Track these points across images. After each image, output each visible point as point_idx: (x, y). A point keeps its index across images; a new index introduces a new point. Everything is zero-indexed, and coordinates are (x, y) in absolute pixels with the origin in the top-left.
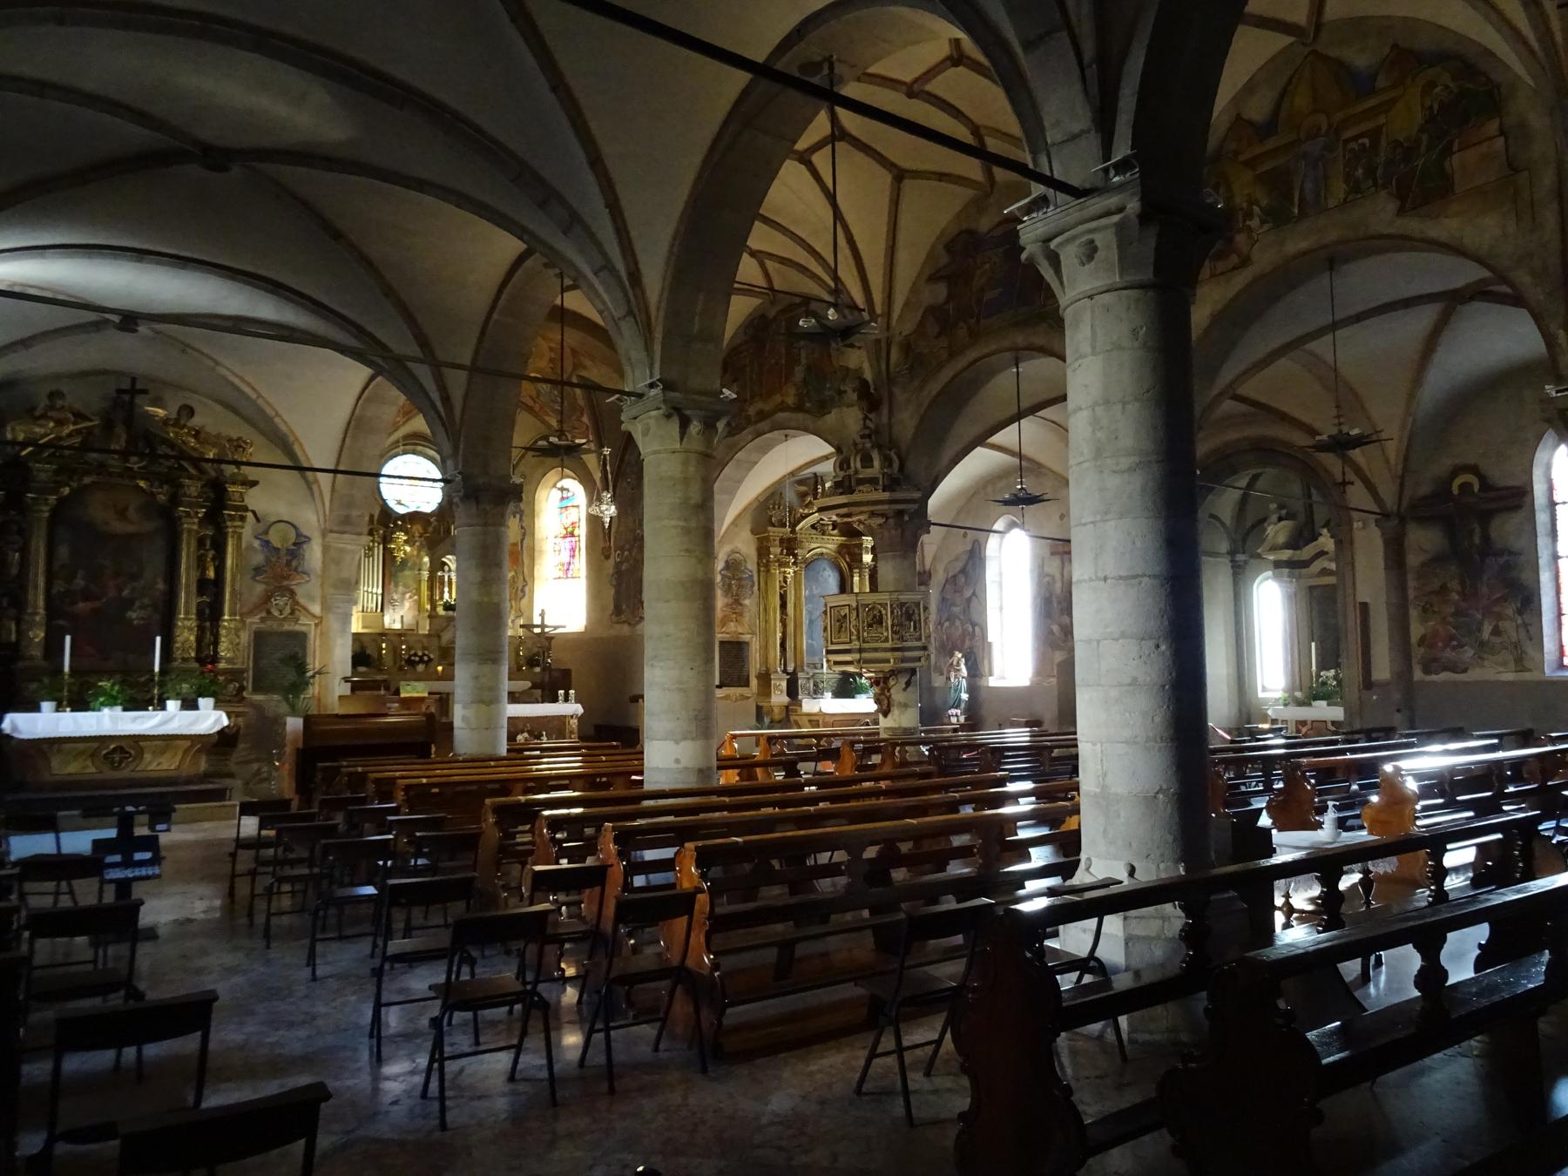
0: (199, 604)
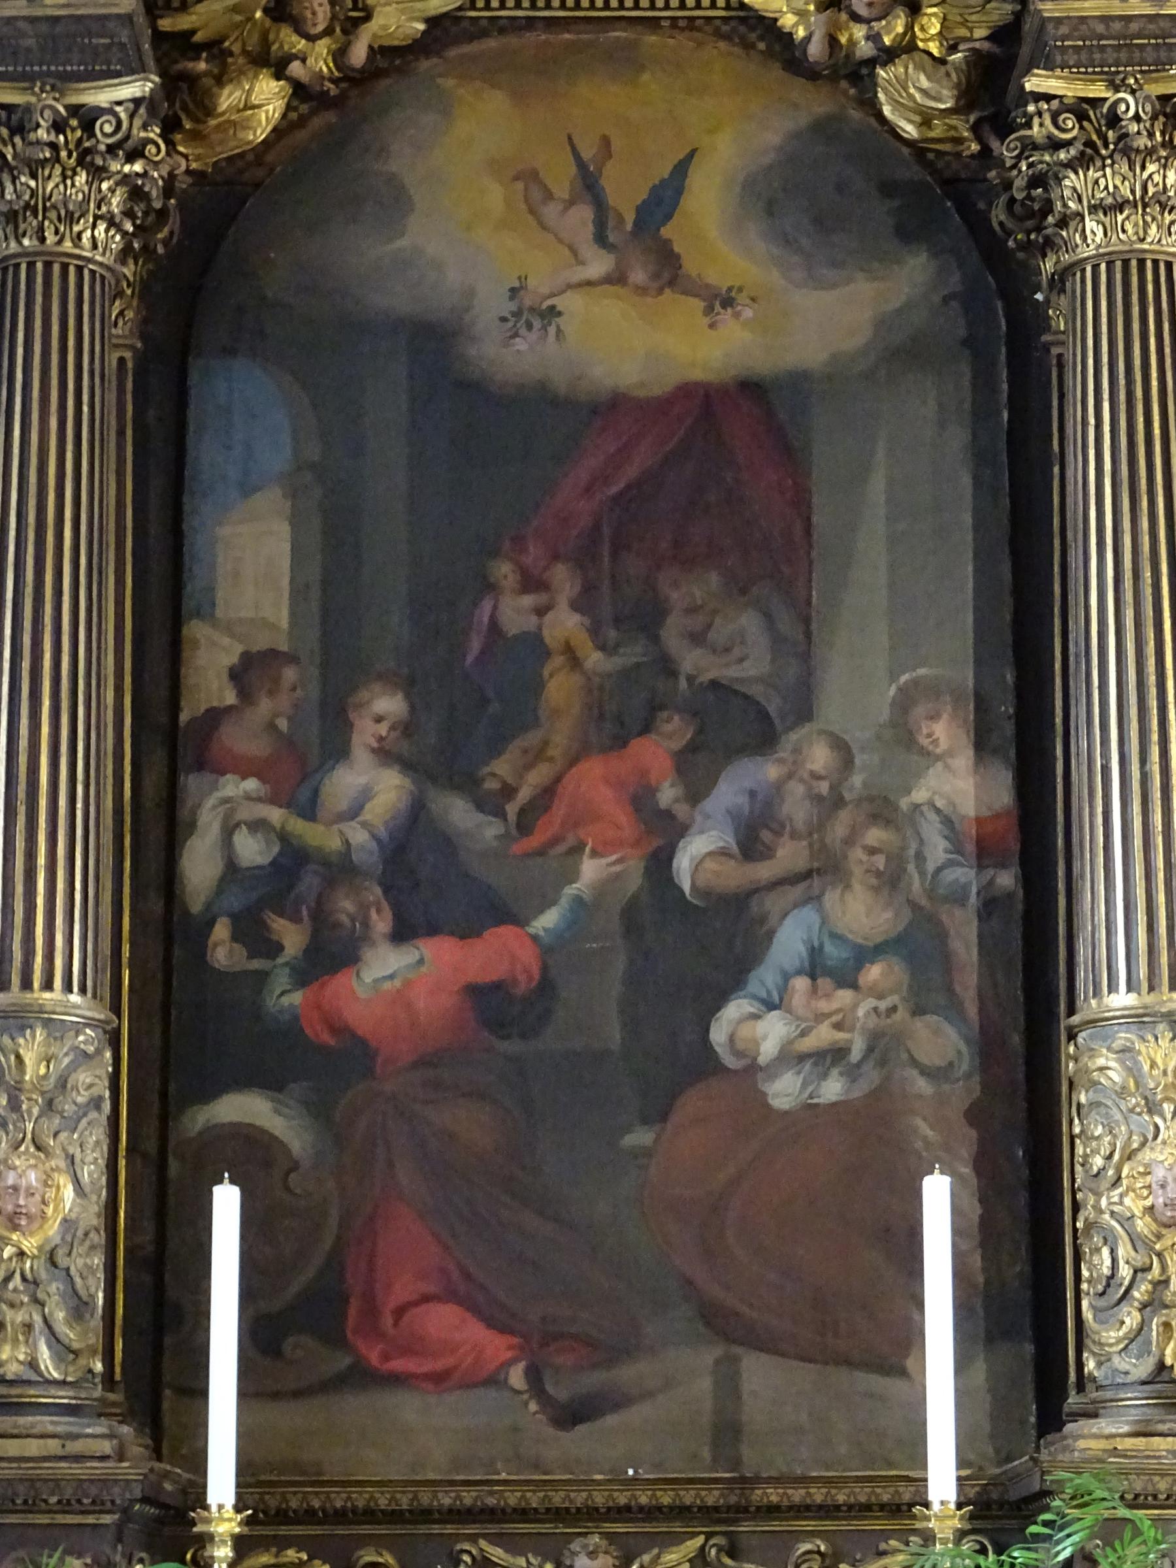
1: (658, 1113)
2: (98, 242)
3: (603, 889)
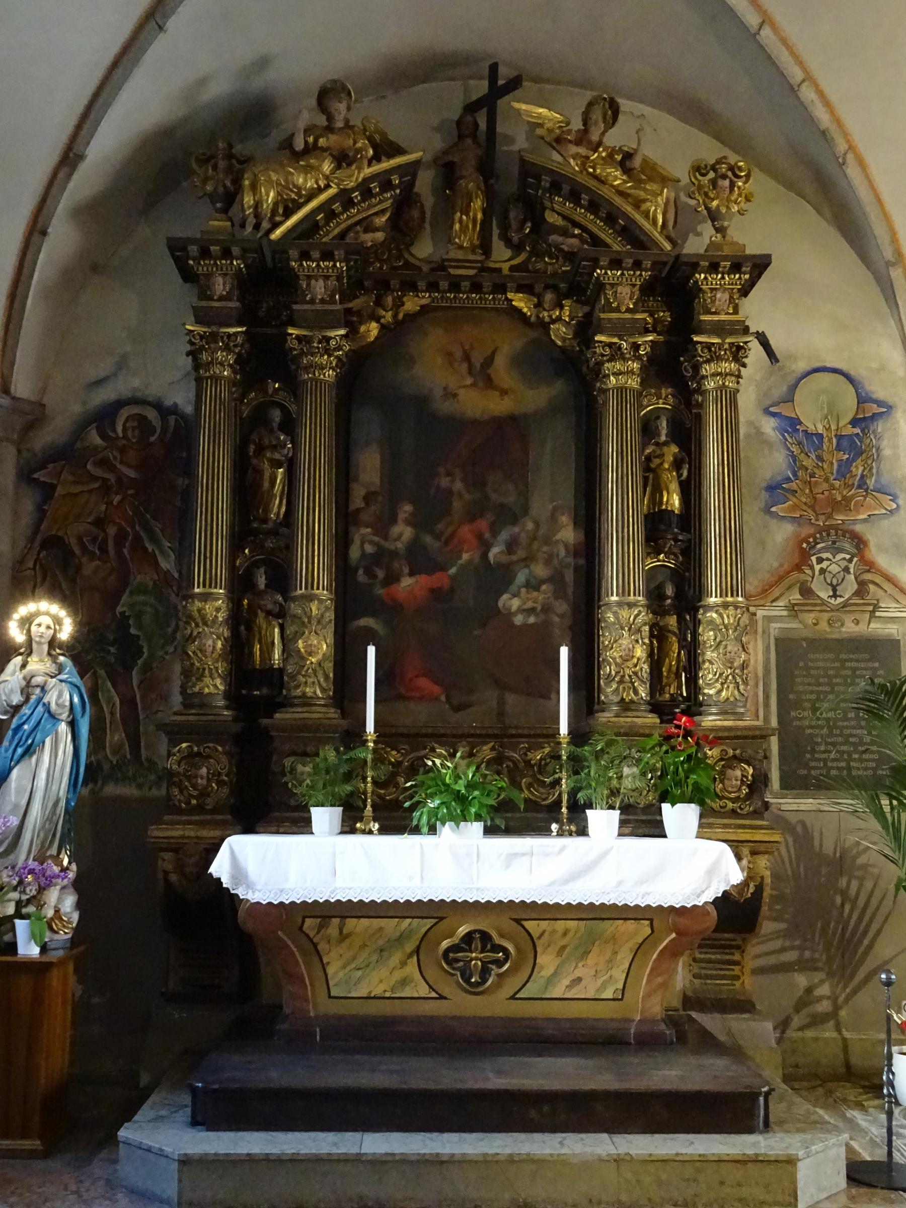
0: (651, 575)
1: (483, 625)
2: (330, 375)
3: (470, 562)
